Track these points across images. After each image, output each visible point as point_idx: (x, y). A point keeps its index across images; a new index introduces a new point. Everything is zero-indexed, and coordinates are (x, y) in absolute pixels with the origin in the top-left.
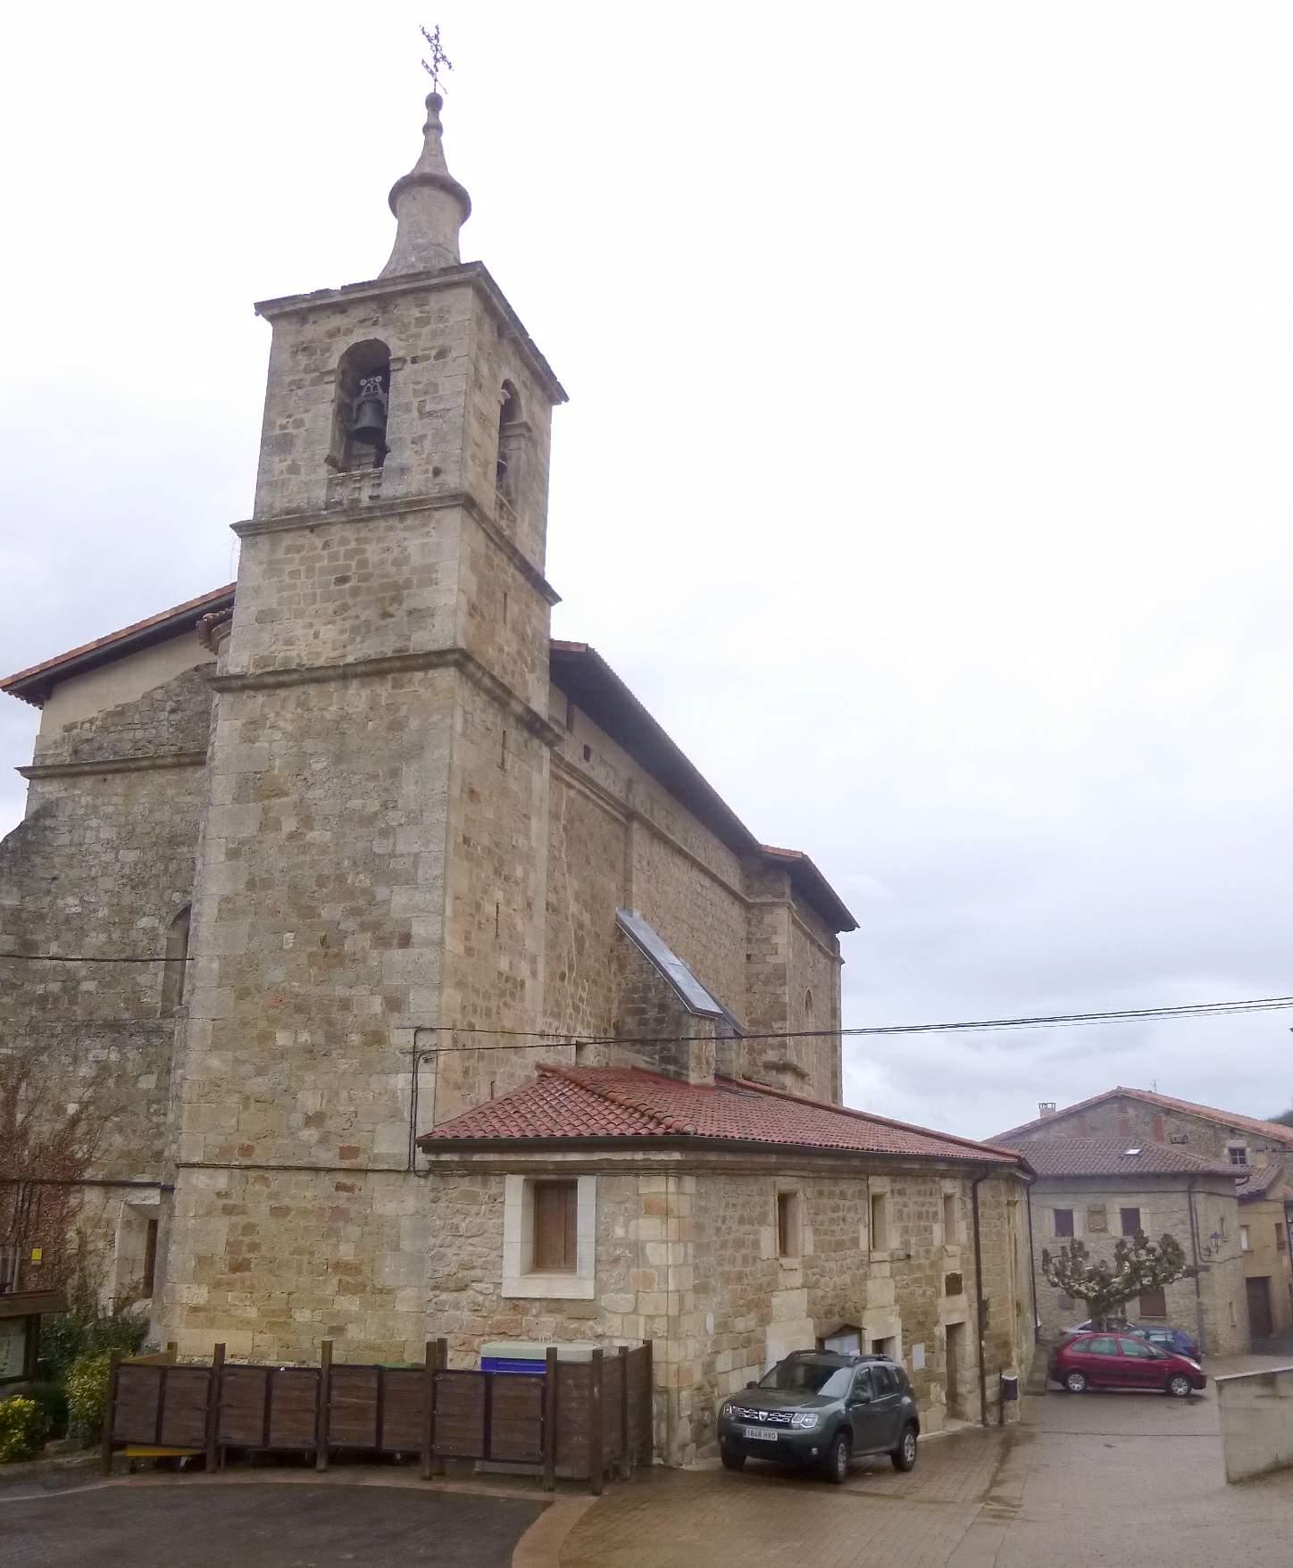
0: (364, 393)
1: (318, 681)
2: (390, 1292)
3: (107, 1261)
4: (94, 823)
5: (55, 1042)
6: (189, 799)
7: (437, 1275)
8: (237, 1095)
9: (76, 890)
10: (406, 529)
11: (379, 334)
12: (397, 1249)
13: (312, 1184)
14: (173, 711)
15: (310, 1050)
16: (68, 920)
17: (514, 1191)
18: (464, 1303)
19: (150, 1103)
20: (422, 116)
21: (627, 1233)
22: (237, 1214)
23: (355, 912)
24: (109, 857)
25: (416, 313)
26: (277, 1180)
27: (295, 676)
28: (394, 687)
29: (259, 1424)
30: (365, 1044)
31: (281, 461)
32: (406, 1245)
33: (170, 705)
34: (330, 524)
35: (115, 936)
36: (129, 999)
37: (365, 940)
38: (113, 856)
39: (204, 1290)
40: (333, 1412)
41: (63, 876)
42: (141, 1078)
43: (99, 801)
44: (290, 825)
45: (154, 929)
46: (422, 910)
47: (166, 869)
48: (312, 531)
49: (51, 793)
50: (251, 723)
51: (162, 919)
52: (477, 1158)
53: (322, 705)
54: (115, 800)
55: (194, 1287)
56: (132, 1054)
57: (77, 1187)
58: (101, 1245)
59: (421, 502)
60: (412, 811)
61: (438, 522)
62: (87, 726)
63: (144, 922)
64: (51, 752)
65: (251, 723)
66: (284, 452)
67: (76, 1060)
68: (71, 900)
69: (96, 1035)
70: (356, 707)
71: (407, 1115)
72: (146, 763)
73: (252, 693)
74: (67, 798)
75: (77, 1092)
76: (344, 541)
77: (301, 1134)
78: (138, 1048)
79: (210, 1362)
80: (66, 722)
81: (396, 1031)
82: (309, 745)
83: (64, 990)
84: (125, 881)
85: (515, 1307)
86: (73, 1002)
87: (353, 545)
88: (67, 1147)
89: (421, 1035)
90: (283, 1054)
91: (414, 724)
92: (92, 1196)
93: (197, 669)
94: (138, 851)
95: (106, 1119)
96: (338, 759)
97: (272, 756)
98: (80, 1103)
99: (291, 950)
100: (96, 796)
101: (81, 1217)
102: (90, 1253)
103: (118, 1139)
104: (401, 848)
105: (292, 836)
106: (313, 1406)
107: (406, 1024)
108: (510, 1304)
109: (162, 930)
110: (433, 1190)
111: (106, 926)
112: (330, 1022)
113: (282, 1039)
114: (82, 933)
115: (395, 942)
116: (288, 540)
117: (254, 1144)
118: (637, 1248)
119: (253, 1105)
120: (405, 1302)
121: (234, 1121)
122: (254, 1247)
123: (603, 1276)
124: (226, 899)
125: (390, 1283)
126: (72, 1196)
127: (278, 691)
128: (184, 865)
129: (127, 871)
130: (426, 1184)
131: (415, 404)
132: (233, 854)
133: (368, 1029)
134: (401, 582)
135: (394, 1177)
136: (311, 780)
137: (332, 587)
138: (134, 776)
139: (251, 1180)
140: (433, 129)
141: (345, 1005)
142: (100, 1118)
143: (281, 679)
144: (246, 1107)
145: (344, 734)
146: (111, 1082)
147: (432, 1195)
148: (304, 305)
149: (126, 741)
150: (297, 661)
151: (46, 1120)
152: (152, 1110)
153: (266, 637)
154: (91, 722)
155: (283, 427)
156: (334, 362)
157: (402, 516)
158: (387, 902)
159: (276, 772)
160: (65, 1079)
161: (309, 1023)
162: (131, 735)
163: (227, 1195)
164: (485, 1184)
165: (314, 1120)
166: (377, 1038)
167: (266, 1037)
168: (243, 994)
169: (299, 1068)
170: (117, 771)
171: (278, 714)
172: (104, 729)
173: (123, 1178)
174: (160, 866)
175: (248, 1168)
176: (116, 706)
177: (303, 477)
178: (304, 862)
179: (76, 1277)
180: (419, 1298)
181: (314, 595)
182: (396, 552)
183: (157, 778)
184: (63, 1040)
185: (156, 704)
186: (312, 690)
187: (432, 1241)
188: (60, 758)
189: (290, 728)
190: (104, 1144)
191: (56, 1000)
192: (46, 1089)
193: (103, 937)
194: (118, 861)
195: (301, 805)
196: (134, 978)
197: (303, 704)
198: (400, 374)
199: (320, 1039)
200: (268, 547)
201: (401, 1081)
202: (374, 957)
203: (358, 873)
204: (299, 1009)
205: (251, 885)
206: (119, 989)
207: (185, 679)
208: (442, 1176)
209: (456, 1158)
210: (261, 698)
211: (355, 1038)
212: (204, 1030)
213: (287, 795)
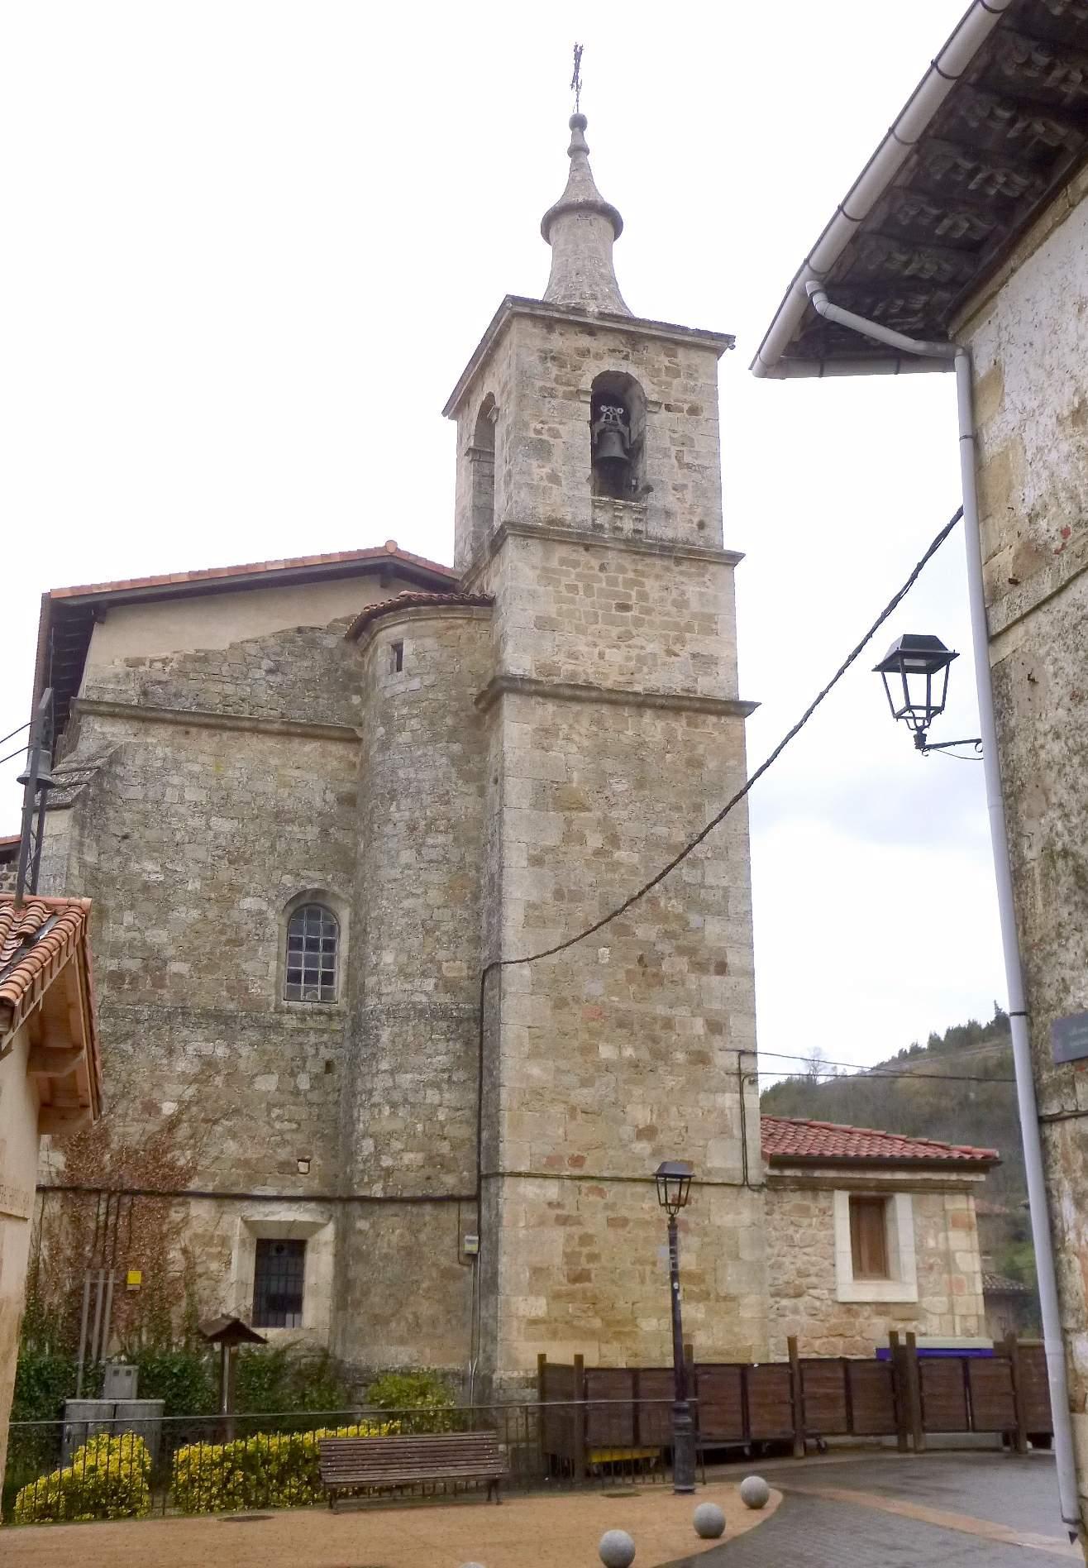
0: (603, 420)
1: (613, 703)
2: (733, 1299)
3: (223, 1285)
4: (176, 780)
5: (141, 1029)
6: (297, 773)
7: (776, 1282)
8: (563, 1106)
9: (156, 854)
10: (681, 573)
11: (633, 371)
12: (737, 1257)
13: (648, 1195)
14: (270, 671)
15: (635, 1065)
16: (146, 887)
17: (841, 1203)
18: (802, 1308)
19: (270, 1106)
20: (566, 138)
21: (937, 1243)
22: (571, 1225)
23: (669, 935)
24: (197, 822)
25: (665, 361)
26: (613, 1191)
27: (594, 694)
28: (689, 725)
29: (738, 1418)
30: (691, 1062)
31: (539, 467)
32: (746, 1255)
33: (267, 664)
34: (607, 548)
35: (211, 915)
36: (233, 987)
37: (683, 963)
38: (203, 822)
39: (543, 1301)
40: (808, 1404)
41: (136, 835)
42: (258, 1079)
43: (182, 756)
44: (595, 841)
45: (261, 912)
46: (735, 942)
47: (273, 846)
48: (587, 549)
49: (113, 735)
50: (543, 730)
51: (270, 902)
52: (817, 1174)
53: (619, 727)
54: (203, 758)
55: (532, 1299)
56: (245, 1051)
57: (180, 1199)
58: (214, 1266)
59: (701, 553)
60: (716, 847)
61: (713, 574)
62: (159, 665)
63: (248, 903)
64: (111, 686)
65: (543, 730)
66: (542, 458)
67: (171, 1052)
68: (149, 866)
69: (197, 1025)
70: (653, 736)
71: (737, 1133)
72: (247, 724)
73: (540, 700)
74: (138, 745)
75: (174, 1089)
76: (622, 569)
77: (633, 1145)
78: (252, 1045)
79: (670, 1363)
80: (134, 654)
81: (720, 1053)
82: (609, 765)
83: (146, 968)
84: (220, 852)
85: (849, 1311)
86: (159, 983)
87: (631, 575)
88: (165, 1152)
89: (743, 1058)
90: (607, 1067)
91: (712, 764)
92: (201, 1211)
93: (300, 630)
94: (236, 821)
95: (216, 1122)
96: (640, 784)
97: (569, 768)
98: (180, 1102)
99: (608, 965)
100: (179, 749)
101: (186, 1234)
102: (200, 1276)
103: (231, 1147)
104: (710, 880)
105: (598, 853)
106: (787, 1398)
107: (729, 1046)
108: (843, 1308)
109: (271, 915)
110: (767, 1204)
111: (199, 900)
112: (654, 1040)
113: (606, 1052)
114: (166, 906)
115: (712, 968)
116: (562, 551)
117: (585, 1154)
118: (948, 1257)
119: (580, 1116)
120: (749, 1309)
121: (561, 1131)
122: (593, 1257)
123: (922, 1280)
124: (532, 906)
125: (733, 1291)
126: (173, 1209)
127: (569, 704)
128: (295, 845)
129: (222, 841)
130: (760, 1198)
131: (674, 450)
132: (536, 861)
133: (691, 1048)
134: (682, 624)
135: (728, 1190)
136: (613, 800)
137: (614, 612)
138: (226, 735)
139: (584, 1191)
140: (578, 151)
141: (668, 1024)
142: (206, 1121)
143: (578, 693)
144: (573, 1117)
145: (643, 760)
146: (219, 1080)
147: (766, 1209)
148: (557, 315)
149: (216, 693)
150: (583, 677)
151: (133, 1120)
152: (273, 1115)
153: (547, 645)
154: (165, 661)
155: (538, 432)
156: (586, 384)
157: (678, 561)
158: (700, 929)
159: (574, 785)
160: (157, 1073)
161: (632, 1038)
162: (218, 688)
163: (559, 1205)
164: (815, 1198)
165: (648, 1133)
166: (701, 1058)
167: (588, 1050)
168: (560, 1004)
169: (626, 1082)
170: (207, 726)
171: (571, 727)
172: (182, 673)
173: (237, 1190)
174: (265, 843)
175: (581, 1178)
176: (197, 651)
177: (565, 490)
178: (613, 880)
179: (184, 1303)
180: (762, 1304)
181: (596, 614)
182: (675, 594)
183: (257, 745)
184: (153, 1027)
185: (249, 659)
186: (605, 710)
187: (769, 1250)
188: (124, 696)
189: (586, 743)
190: (213, 1152)
191: (134, 980)
192: (130, 1083)
193: (195, 914)
194: (210, 828)
195: (604, 824)
196: (238, 965)
197: (598, 722)
198: (656, 417)
199: (645, 1055)
200: (540, 554)
201: (729, 1100)
202: (692, 981)
203: (670, 898)
204: (621, 1024)
205: (559, 895)
206: (219, 975)
207: (285, 638)
208: (776, 1191)
209: (798, 1173)
210: (551, 707)
211: (680, 1056)
212: (519, 1036)
213: (589, 810)
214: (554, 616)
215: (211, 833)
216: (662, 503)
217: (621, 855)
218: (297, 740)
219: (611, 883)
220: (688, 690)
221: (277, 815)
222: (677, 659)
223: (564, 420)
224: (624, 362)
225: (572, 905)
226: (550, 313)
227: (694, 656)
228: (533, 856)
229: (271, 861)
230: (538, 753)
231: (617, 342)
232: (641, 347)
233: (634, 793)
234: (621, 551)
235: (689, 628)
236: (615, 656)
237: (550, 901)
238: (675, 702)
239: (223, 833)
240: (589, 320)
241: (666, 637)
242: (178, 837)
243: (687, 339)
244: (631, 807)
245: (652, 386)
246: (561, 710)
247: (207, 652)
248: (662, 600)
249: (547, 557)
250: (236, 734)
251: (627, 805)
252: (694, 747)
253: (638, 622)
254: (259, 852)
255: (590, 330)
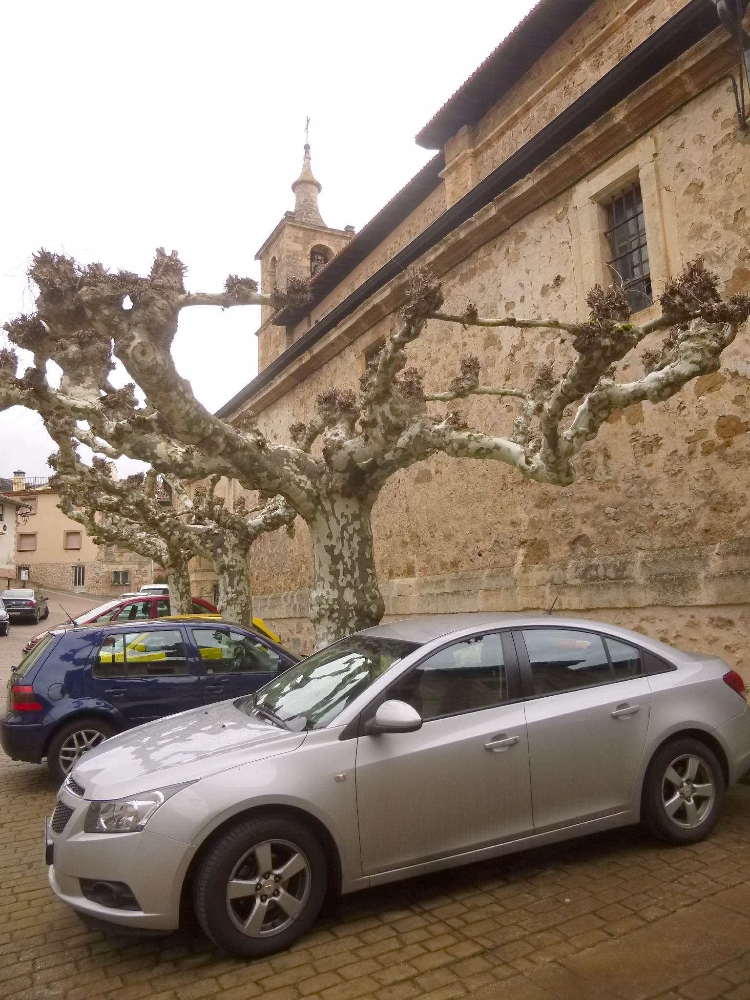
140: (307, 157)
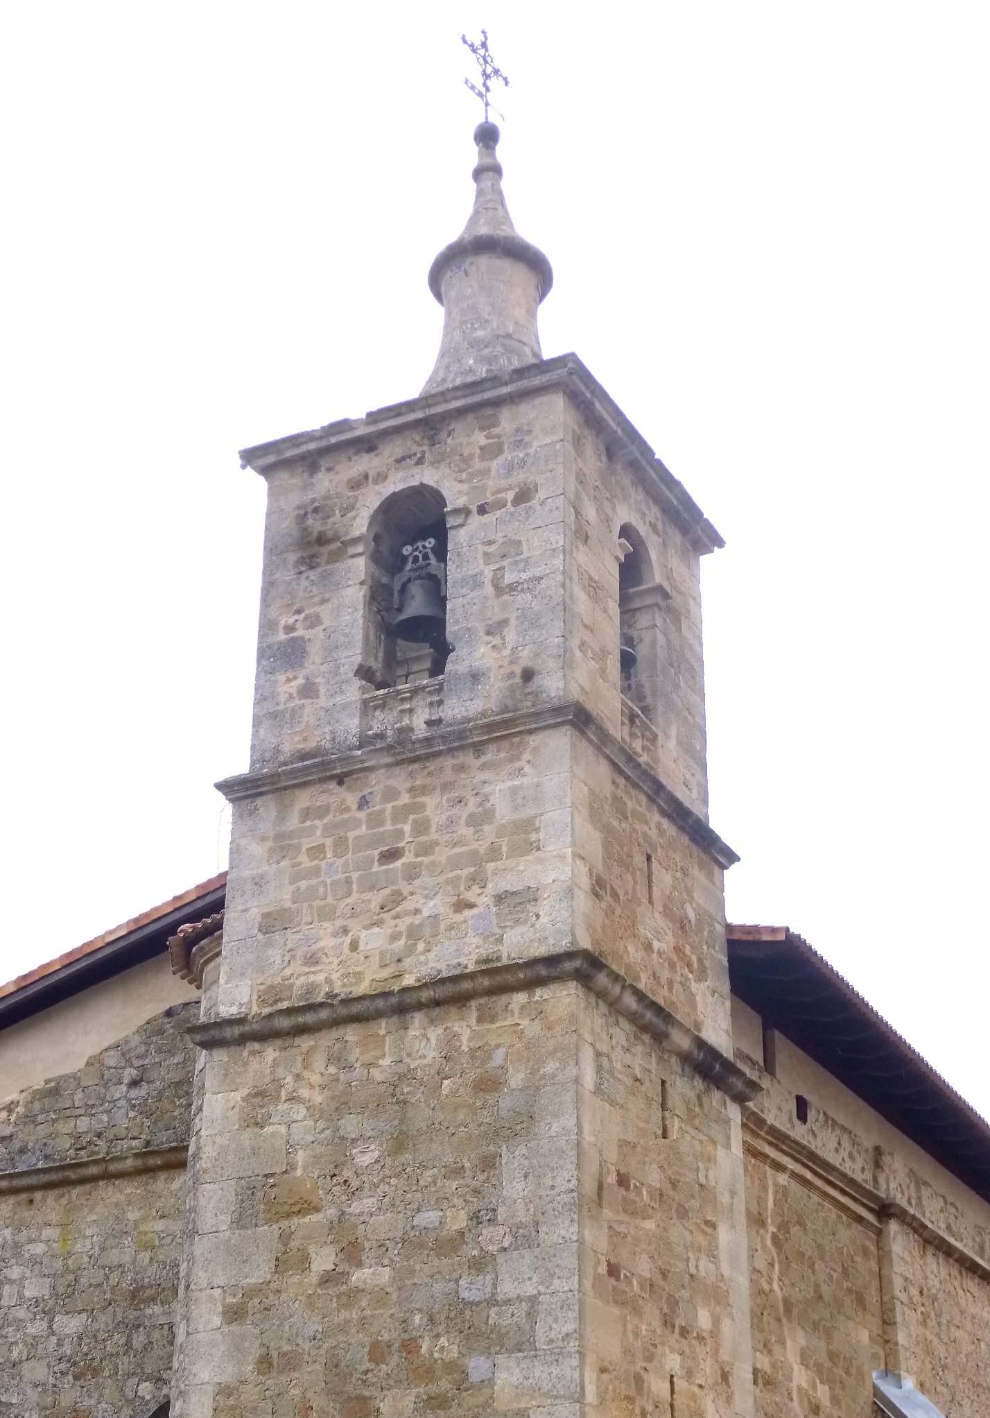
0: (409, 566)
10: (484, 767)
11: (428, 476)
14: (134, 1083)
24: (37, 1328)
25: (481, 439)
27: (324, 1014)
28: (480, 1020)
33: (129, 1074)
43: (23, 1237)
44: (323, 1260)
46: (547, 1395)
47: (128, 1344)
48: (340, 783)
50: (257, 1095)
53: (369, 1057)
54: (47, 1232)
60: (520, 1225)
65: (257, 1095)
66: (292, 667)
73: (256, 1046)
82: (350, 1125)
84: (63, 1366)
91: (516, 1078)
93: (169, 1013)
94: (84, 1316)
104: (507, 1289)
105: (327, 1279)
127: (297, 1041)
129: (67, 1349)
131: (488, 573)
132: (234, 1314)
136: (355, 1183)
137: (376, 868)
138: (76, 1191)
140: (487, 172)
155: (290, 629)
157: (478, 748)
158: (489, 1382)
159: (299, 1172)
171: (298, 1077)
172: (29, 1119)
174: (119, 1339)
176: (47, 1082)
177: (323, 701)
182: (472, 806)
183: (111, 1195)
185: (107, 1074)
186: (351, 1034)
189: (318, 1099)
194: (53, 1333)
198: (462, 532)
203: (438, 1336)
205: (265, 1364)
207: (152, 1030)
210: (271, 1053)
213: (317, 1210)
214: (288, 904)
215: (54, 1339)
216: (466, 663)
217: (360, 1276)
218: (162, 1176)
219: (343, 1328)
220: (487, 961)
221: (134, 1295)
222: (474, 911)
223: (327, 596)
224: (417, 470)
225: (283, 1378)
226: (304, 448)
227: (499, 899)
228: (231, 1306)
229: (125, 1364)
230: (247, 1137)
231: (409, 443)
232: (443, 435)
233: (389, 1161)
234: (388, 766)
235: (494, 853)
236: (374, 940)
237: (252, 1377)
238: (449, 989)
239: (67, 1336)
240: (357, 433)
241: (454, 882)
242: (15, 1355)
243: (504, 390)
244: (384, 1187)
245: (459, 486)
246: (284, 1054)
247: (59, 1080)
248: (452, 821)
249: (282, 818)
250: (88, 1187)
251: (376, 1186)
252: (489, 1057)
253: (412, 873)
254: (111, 1355)
255: (366, 444)
